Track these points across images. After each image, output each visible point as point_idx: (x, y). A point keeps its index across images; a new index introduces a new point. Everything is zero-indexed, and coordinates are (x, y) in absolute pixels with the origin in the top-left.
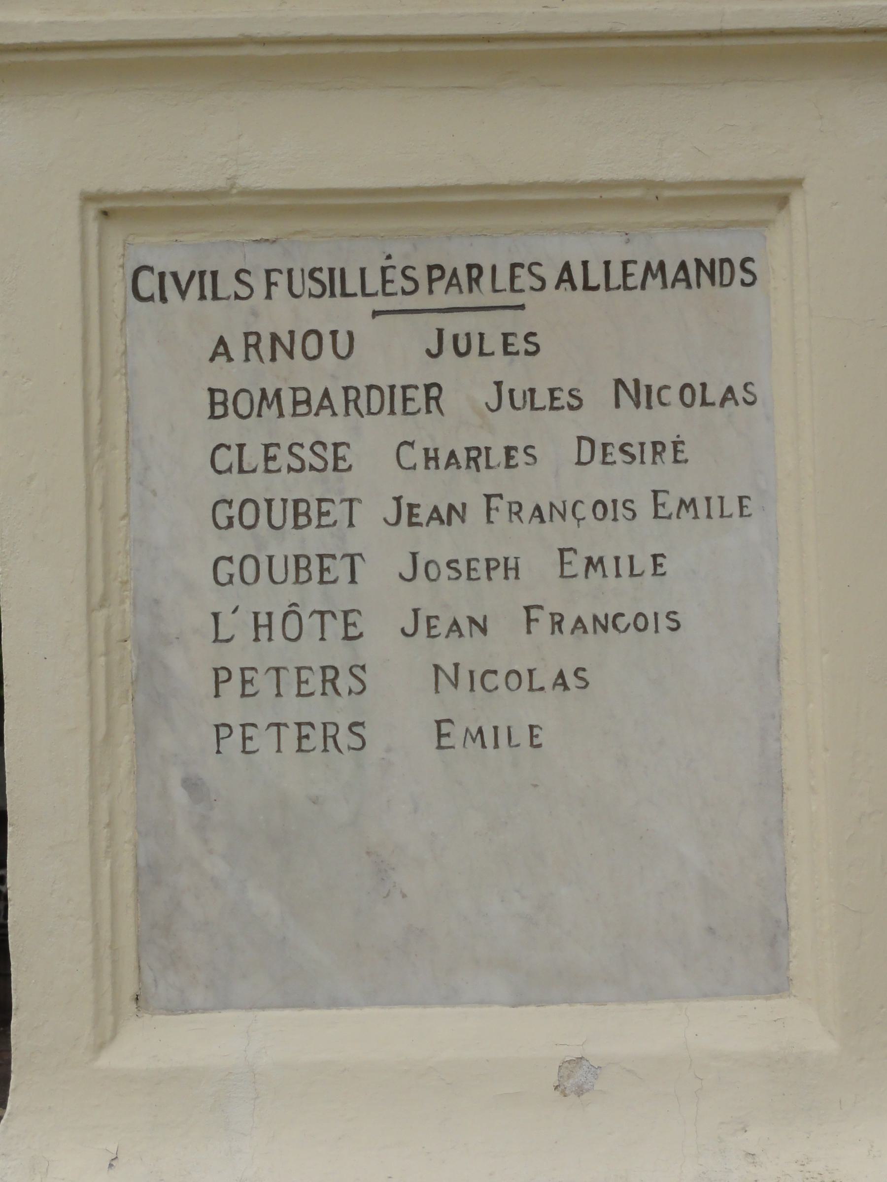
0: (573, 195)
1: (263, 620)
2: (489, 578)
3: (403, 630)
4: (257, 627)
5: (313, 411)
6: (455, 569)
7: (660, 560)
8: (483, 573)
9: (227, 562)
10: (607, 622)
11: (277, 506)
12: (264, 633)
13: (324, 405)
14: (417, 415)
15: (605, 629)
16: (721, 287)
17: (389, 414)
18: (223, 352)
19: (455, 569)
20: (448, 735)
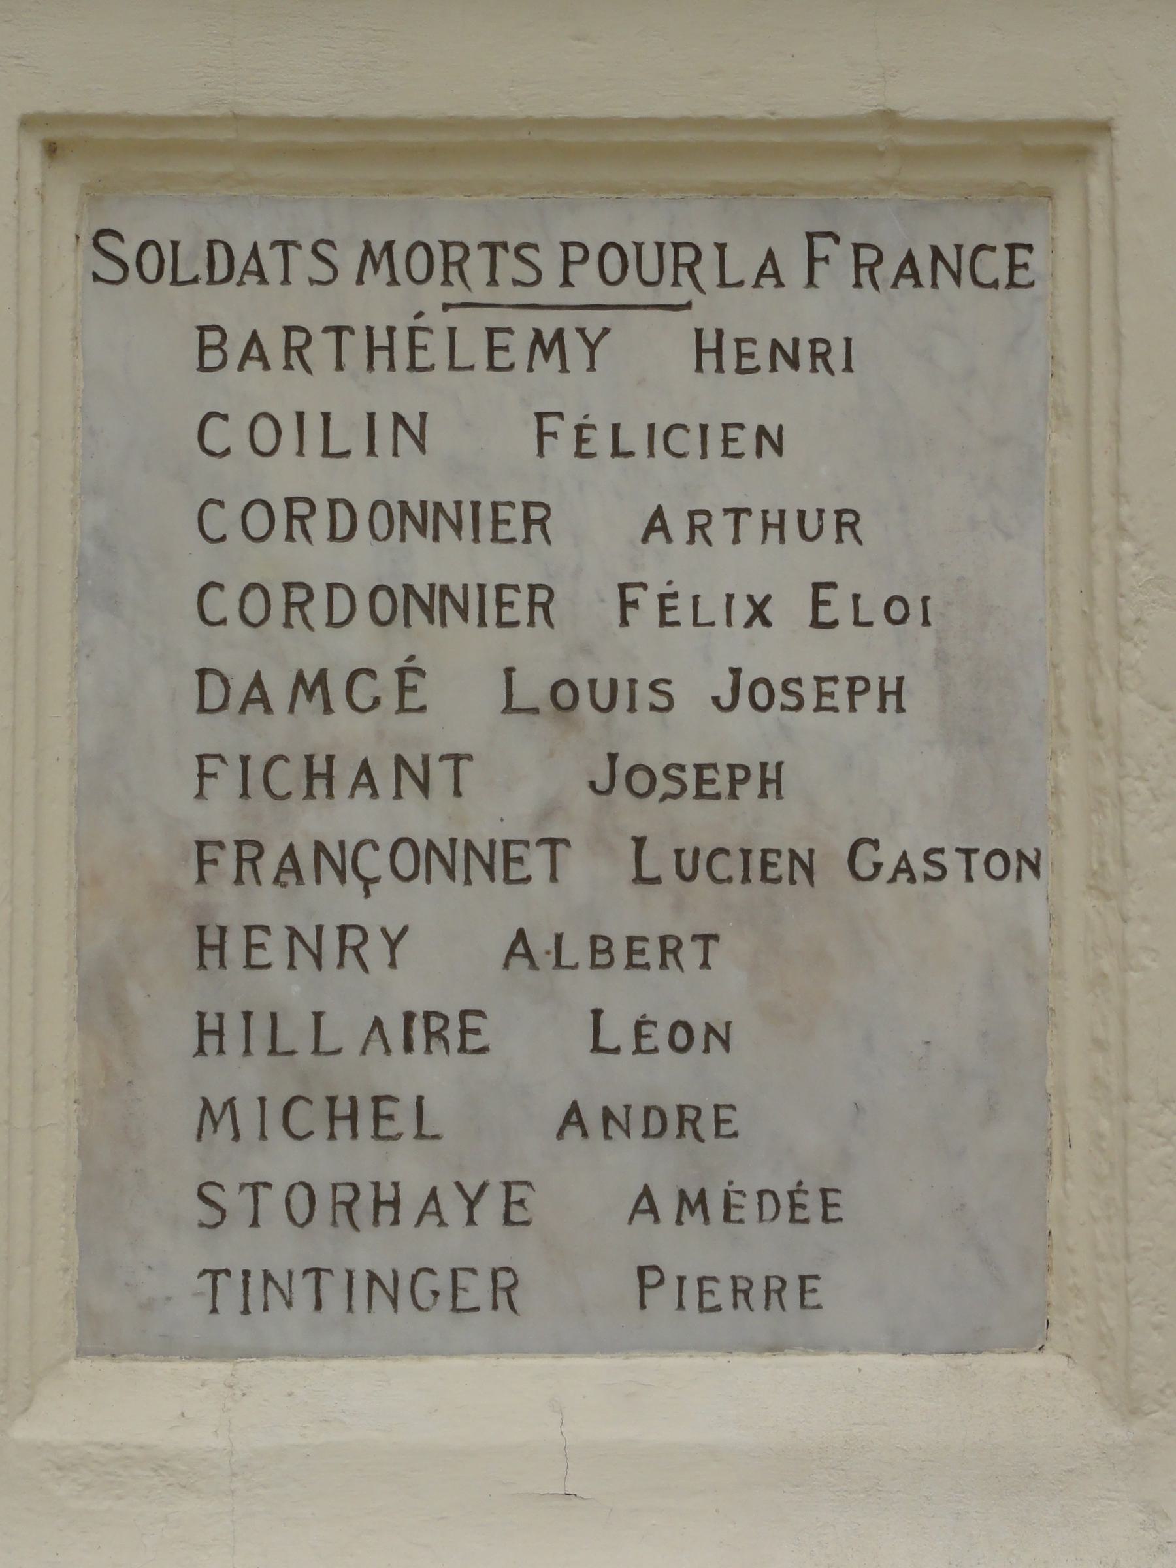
0: (731, 137)
1: (709, 342)
2: (853, 708)
3: (592, 785)
4: (700, 351)
5: (411, 663)
6: (677, 780)
7: (832, 1199)
8: (841, 700)
9: (392, 1219)
10: (1019, 870)
11: (650, 254)
12: (709, 360)
13: (250, 268)
14: (519, 1279)
15: (1021, 855)
16: (498, 627)
17: (694, 798)
18: (648, 1207)
19: (677, 780)
20: (1025, 266)
